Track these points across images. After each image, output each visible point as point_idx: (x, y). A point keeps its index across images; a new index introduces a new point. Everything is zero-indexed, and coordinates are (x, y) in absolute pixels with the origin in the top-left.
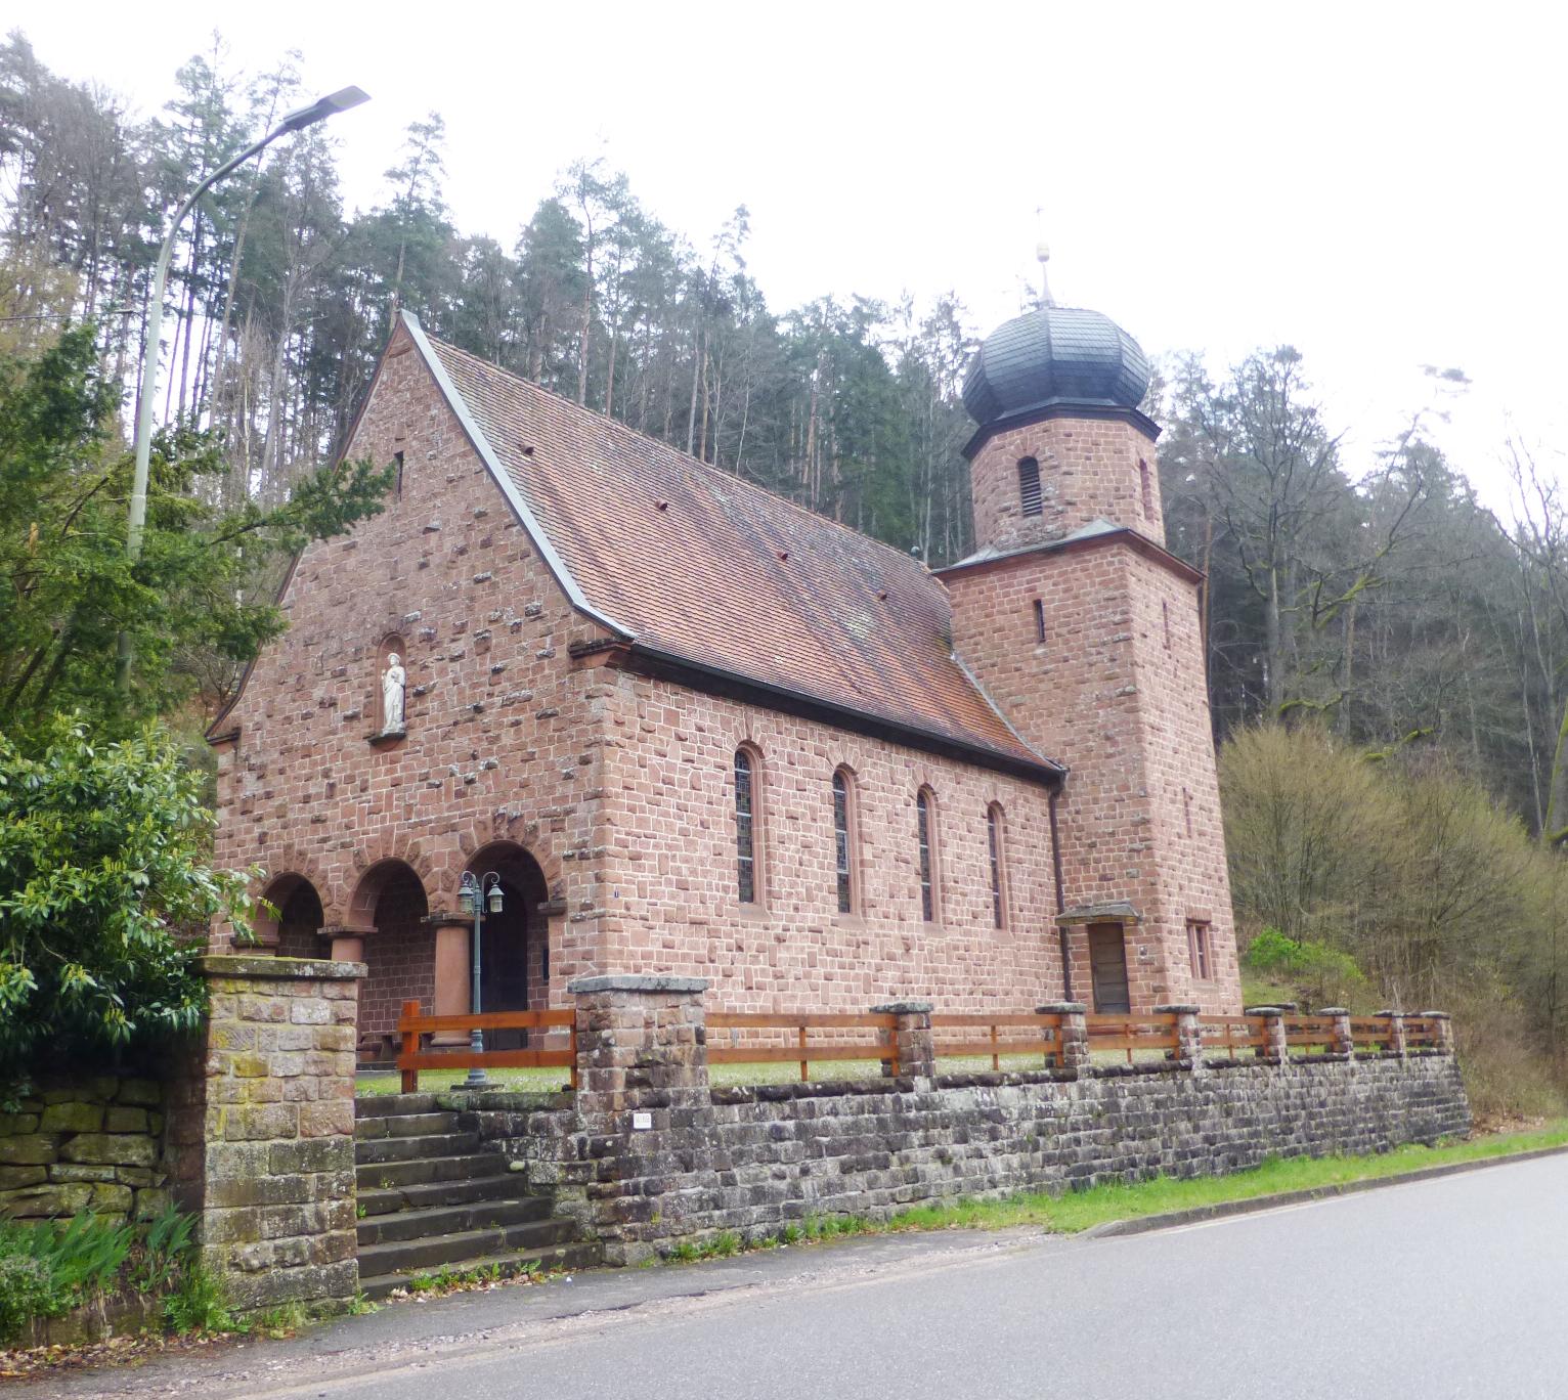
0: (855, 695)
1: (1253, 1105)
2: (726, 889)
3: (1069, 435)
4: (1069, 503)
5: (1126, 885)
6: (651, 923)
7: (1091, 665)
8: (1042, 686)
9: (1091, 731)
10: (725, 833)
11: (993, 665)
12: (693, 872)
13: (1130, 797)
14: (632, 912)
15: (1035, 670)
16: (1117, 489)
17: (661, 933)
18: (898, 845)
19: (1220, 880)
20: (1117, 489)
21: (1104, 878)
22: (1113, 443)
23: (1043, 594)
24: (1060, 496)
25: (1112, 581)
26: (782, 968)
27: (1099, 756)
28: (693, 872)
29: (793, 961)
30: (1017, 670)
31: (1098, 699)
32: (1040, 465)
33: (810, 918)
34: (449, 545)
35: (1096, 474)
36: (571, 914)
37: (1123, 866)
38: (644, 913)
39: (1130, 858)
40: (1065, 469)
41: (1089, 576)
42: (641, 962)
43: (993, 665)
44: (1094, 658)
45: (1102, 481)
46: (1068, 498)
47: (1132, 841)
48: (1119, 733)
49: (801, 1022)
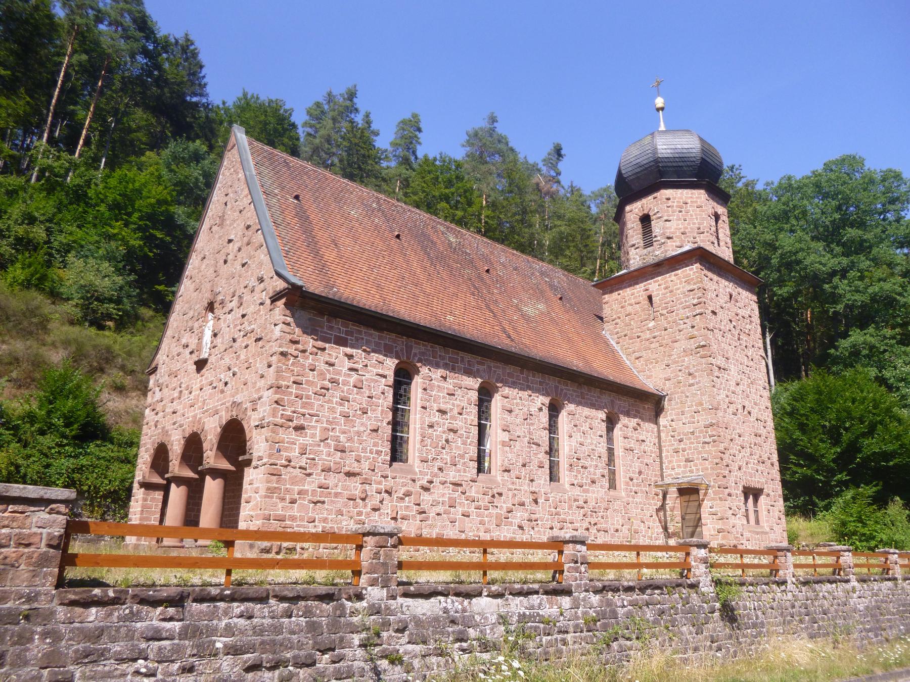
0: (507, 341)
1: (759, 613)
2: (379, 453)
3: (668, 199)
4: (669, 238)
5: (701, 464)
6: (308, 471)
7: (680, 331)
8: (653, 346)
9: (680, 370)
10: (382, 414)
11: (625, 336)
12: (350, 440)
13: (704, 410)
14: (292, 464)
15: (648, 336)
16: (699, 229)
17: (319, 478)
18: (530, 433)
19: (772, 465)
20: (699, 229)
21: (687, 460)
22: (696, 202)
23: (653, 291)
24: (663, 234)
25: (692, 279)
26: (424, 506)
27: (685, 386)
28: (350, 440)
29: (435, 504)
30: (638, 337)
31: (684, 351)
32: (652, 218)
33: (452, 475)
34: (236, 245)
35: (685, 220)
36: (254, 463)
37: (699, 453)
38: (303, 464)
39: (703, 447)
40: (666, 218)
41: (679, 279)
42: (297, 496)
43: (625, 336)
44: (682, 327)
45: (689, 224)
46: (668, 235)
47: (705, 437)
48: (696, 371)
49: (485, 546)
